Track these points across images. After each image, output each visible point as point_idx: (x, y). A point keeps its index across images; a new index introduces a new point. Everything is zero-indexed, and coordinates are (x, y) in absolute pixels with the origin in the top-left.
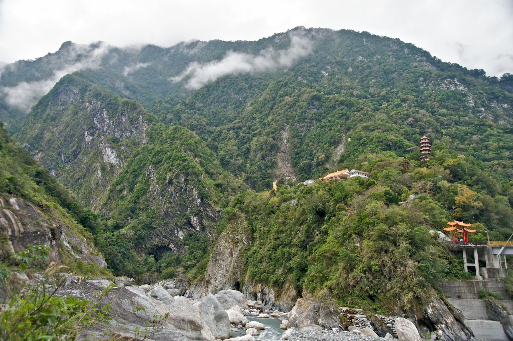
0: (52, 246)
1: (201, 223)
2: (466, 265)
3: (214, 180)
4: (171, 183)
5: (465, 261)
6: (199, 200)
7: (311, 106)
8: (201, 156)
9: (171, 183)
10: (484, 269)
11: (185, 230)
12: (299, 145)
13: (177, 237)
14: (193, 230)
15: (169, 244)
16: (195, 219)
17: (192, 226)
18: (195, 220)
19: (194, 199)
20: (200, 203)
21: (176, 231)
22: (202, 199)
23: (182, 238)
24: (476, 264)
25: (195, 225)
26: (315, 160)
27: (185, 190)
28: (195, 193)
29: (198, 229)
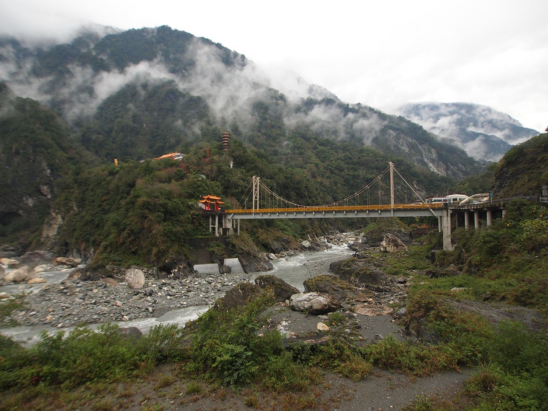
0: (485, 293)
1: (52, 192)
2: (211, 226)
3: (67, 153)
4: (17, 153)
5: (210, 224)
6: (49, 171)
7: (168, 99)
8: (53, 130)
9: (17, 153)
10: (221, 229)
11: (35, 198)
12: (155, 130)
13: (27, 204)
14: (44, 198)
15: (52, 208)
16: (45, 187)
17: (42, 194)
18: (45, 189)
19: (44, 170)
20: (50, 174)
21: (25, 199)
22: (52, 170)
23: (31, 205)
24: (216, 226)
25: (45, 193)
26: (167, 144)
27: (34, 161)
28: (44, 164)
29: (49, 197)
